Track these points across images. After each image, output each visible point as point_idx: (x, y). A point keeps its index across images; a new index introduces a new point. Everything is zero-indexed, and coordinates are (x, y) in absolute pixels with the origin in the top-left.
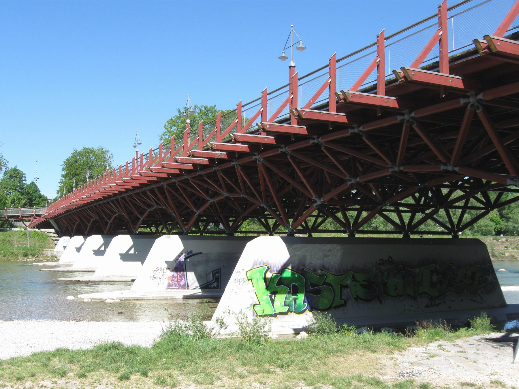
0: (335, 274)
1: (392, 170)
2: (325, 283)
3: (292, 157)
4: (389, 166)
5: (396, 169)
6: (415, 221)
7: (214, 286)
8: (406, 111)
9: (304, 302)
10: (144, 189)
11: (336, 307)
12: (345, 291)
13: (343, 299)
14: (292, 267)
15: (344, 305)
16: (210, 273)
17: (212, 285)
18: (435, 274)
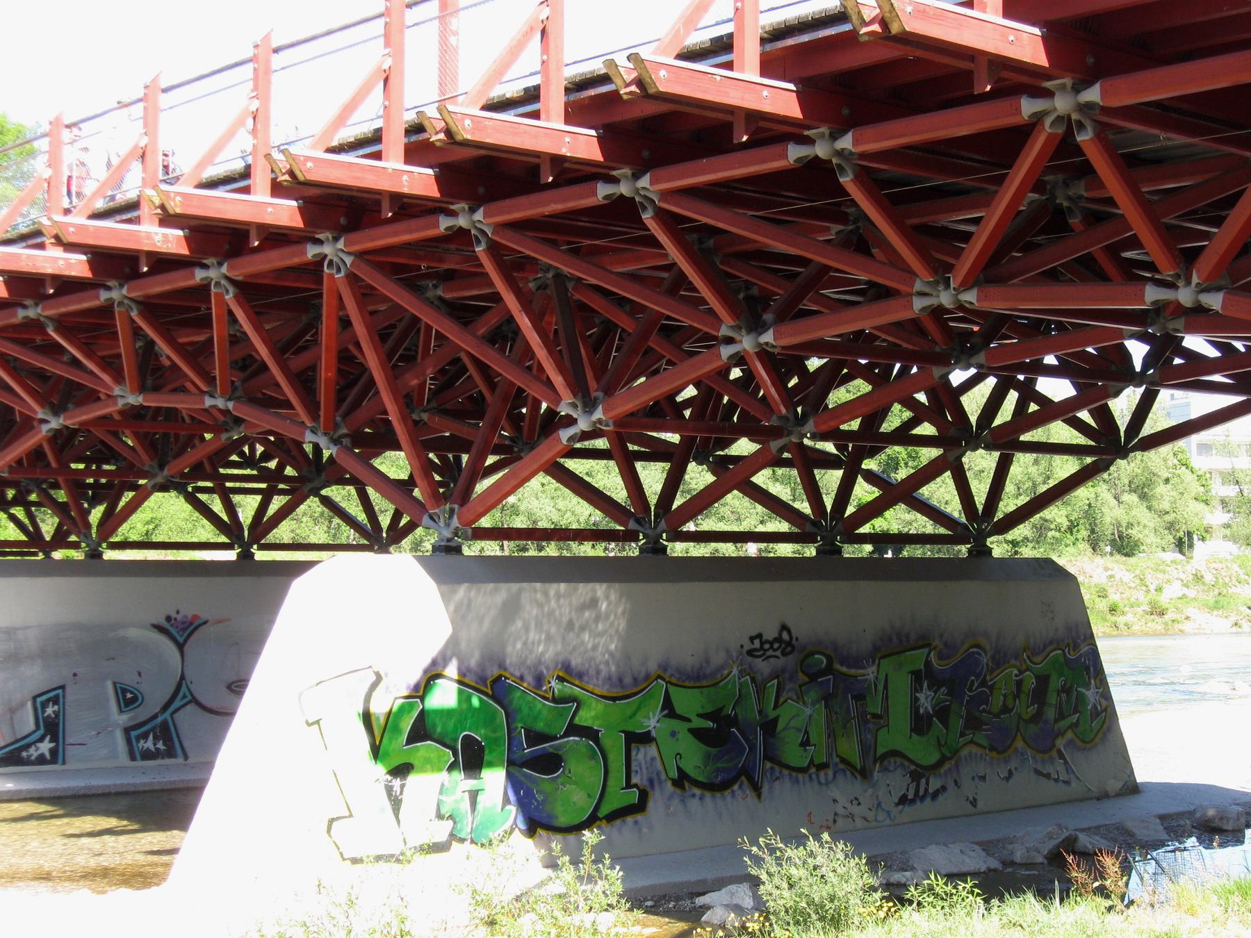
0: (605, 694)
1: (926, 302)
2: (573, 729)
3: (495, 249)
4: (918, 286)
5: (945, 299)
6: (980, 489)
7: (39, 752)
8: (627, 171)
9: (506, 801)
10: (32, 312)
11: (612, 817)
12: (641, 756)
13: (636, 786)
14: (462, 673)
15: (639, 807)
16: (23, 704)
17: (33, 748)
18: (925, 685)
